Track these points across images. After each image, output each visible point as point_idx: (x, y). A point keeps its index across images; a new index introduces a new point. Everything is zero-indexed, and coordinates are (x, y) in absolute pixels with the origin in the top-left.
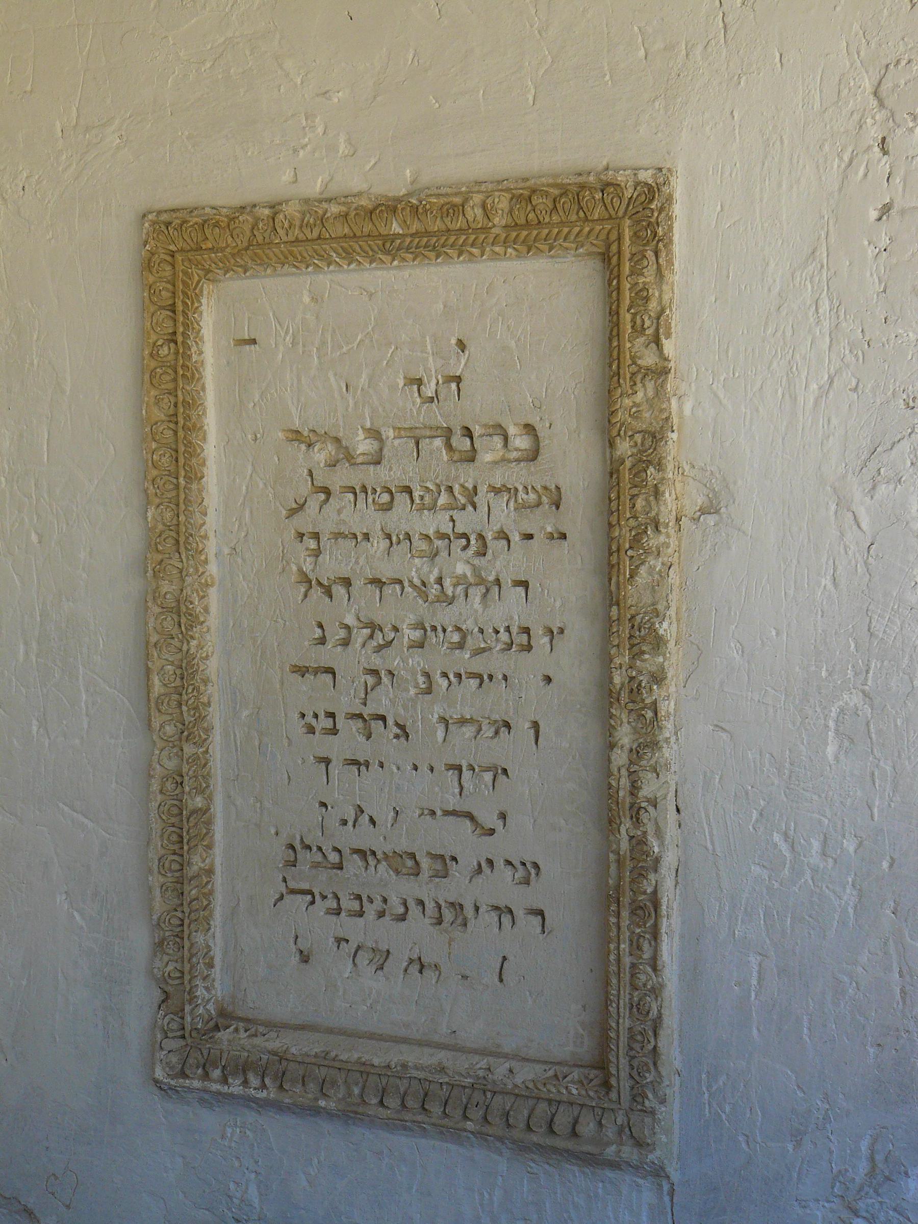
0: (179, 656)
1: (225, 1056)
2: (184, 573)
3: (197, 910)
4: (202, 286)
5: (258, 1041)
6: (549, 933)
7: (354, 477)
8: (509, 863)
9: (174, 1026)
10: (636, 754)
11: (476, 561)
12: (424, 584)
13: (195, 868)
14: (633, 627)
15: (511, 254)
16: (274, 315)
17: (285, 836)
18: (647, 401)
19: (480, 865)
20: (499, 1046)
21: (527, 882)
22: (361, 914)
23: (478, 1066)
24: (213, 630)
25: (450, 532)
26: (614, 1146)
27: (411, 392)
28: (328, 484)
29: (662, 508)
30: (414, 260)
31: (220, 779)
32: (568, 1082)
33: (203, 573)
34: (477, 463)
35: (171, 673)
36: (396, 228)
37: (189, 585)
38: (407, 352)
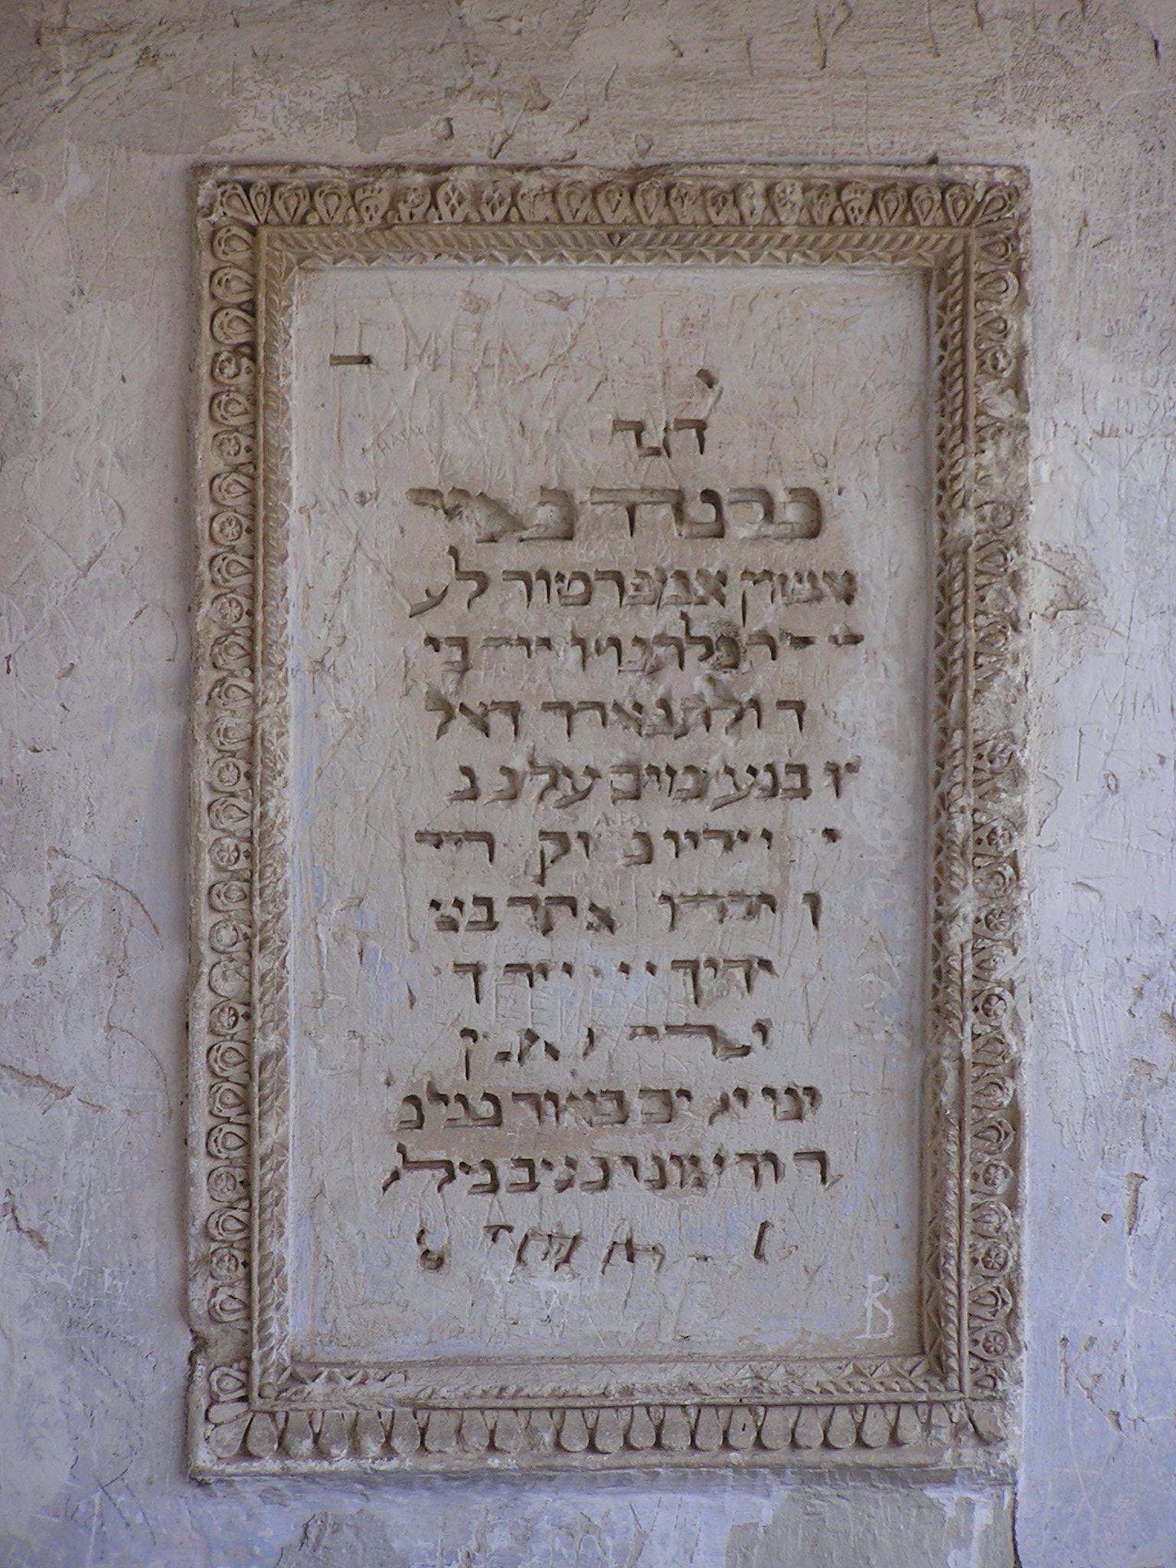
0: (246, 823)
2: (259, 700)
4: (294, 277)
6: (833, 1183)
7: (529, 558)
8: (768, 1092)
10: (987, 923)
11: (724, 677)
12: (638, 707)
14: (980, 756)
15: (796, 261)
18: (998, 463)
22: (533, 1186)
25: (681, 634)
29: (1025, 602)
30: (648, 260)
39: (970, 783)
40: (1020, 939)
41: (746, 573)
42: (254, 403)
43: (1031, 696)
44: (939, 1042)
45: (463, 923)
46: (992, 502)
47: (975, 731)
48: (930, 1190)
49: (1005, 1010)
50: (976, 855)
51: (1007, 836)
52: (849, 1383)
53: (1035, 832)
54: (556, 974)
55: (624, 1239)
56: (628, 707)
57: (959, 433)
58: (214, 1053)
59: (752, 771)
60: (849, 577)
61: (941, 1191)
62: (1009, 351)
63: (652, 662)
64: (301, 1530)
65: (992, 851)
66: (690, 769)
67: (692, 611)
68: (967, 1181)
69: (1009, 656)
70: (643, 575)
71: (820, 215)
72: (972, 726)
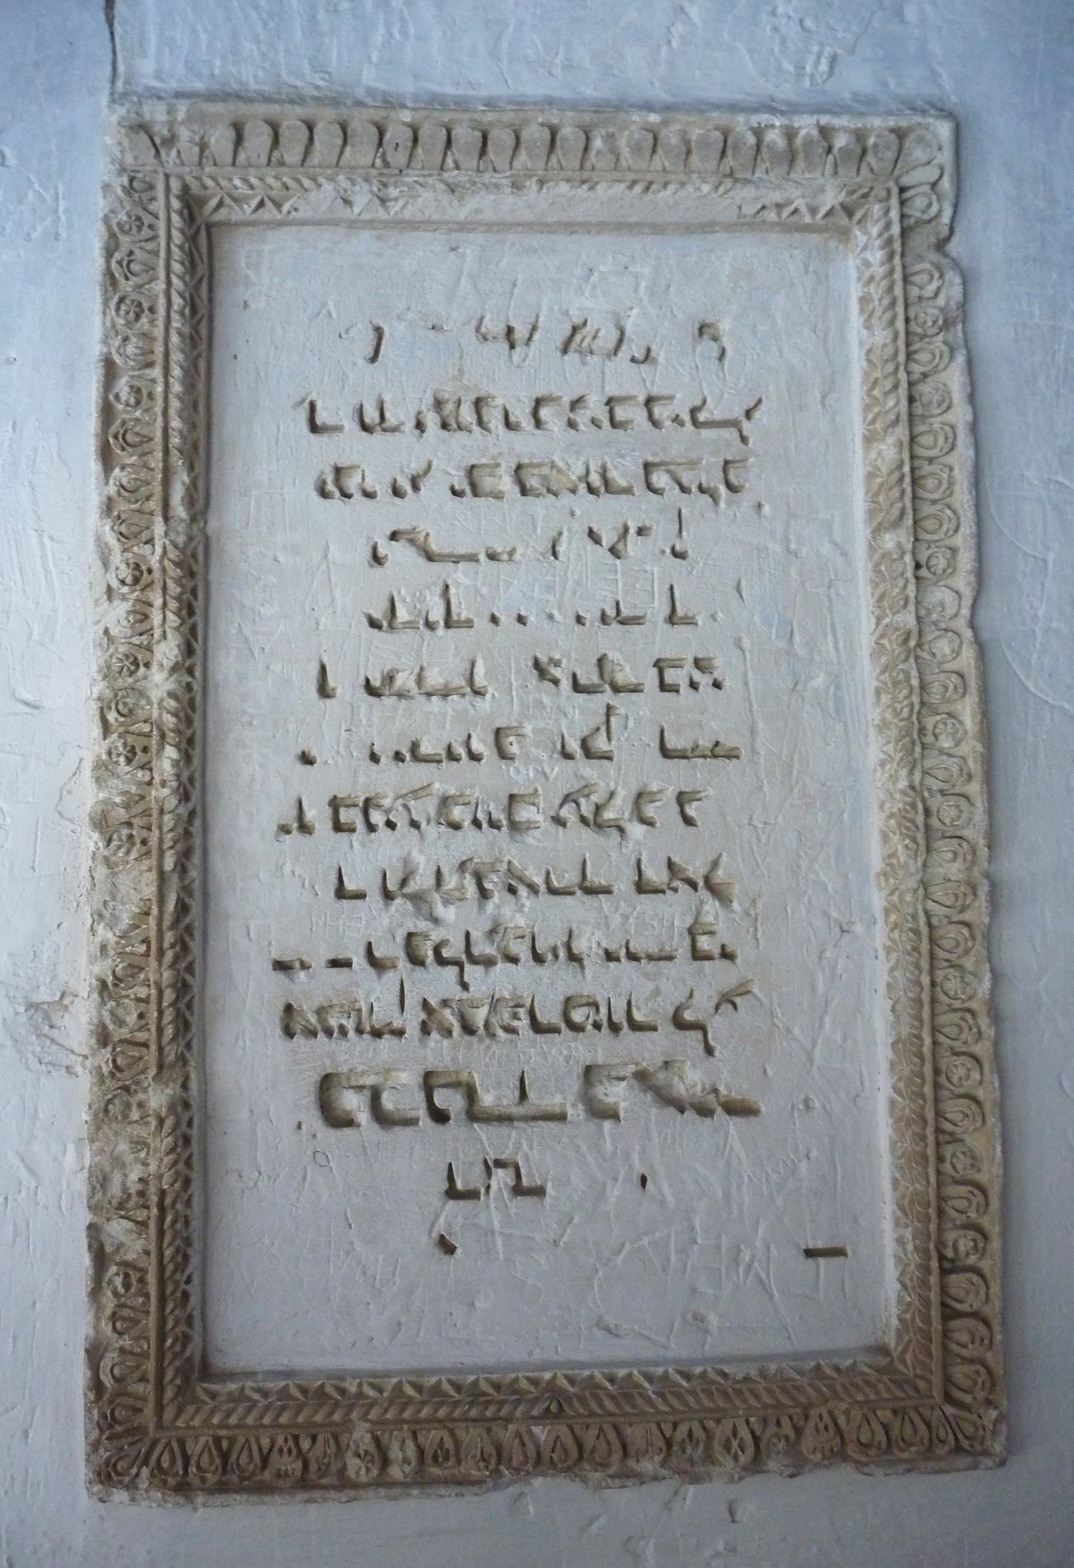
0: (928, 764)
1: (829, 169)
2: (921, 892)
3: (886, 377)
4: (897, 1345)
5: (777, 197)
8: (369, 495)
9: (919, 203)
11: (423, 925)
12: (512, 890)
13: (891, 440)
16: (771, 1297)
17: (745, 504)
19: (416, 488)
20: (379, 238)
21: (338, 471)
22: (610, 402)
23: (401, 203)
24: (875, 807)
26: (179, 119)
27: (530, 1175)
28: (679, 1036)
30: (516, 1380)
31: (861, 580)
32: (254, 196)
33: (892, 893)
34: (420, 1070)
35: (942, 737)
36: (541, 1432)
37: (912, 875)
38: (537, 1237)
39: (155, 813)
40: (100, 645)
41: (399, 1033)
42: (941, 1212)
43: (88, 908)
44: (190, 539)
45: (689, 665)
46: (130, 1123)
47: (150, 870)
48: (201, 387)
49: (117, 568)
50: (148, 735)
51: (114, 756)
52: (287, 188)
53: (84, 763)
54: (591, 615)
55: (518, 349)
56: (523, 891)
57: (168, 1201)
58: (953, 525)
59: (390, 825)
60: (289, 1033)
61: (189, 384)
62: (110, 1294)
63: (497, 938)
64: (837, 70)
65: (130, 739)
66: (456, 826)
67: (457, 993)
68: (159, 389)
69: (112, 953)
70: (510, 1030)
71: (326, 1442)
72: (153, 876)
